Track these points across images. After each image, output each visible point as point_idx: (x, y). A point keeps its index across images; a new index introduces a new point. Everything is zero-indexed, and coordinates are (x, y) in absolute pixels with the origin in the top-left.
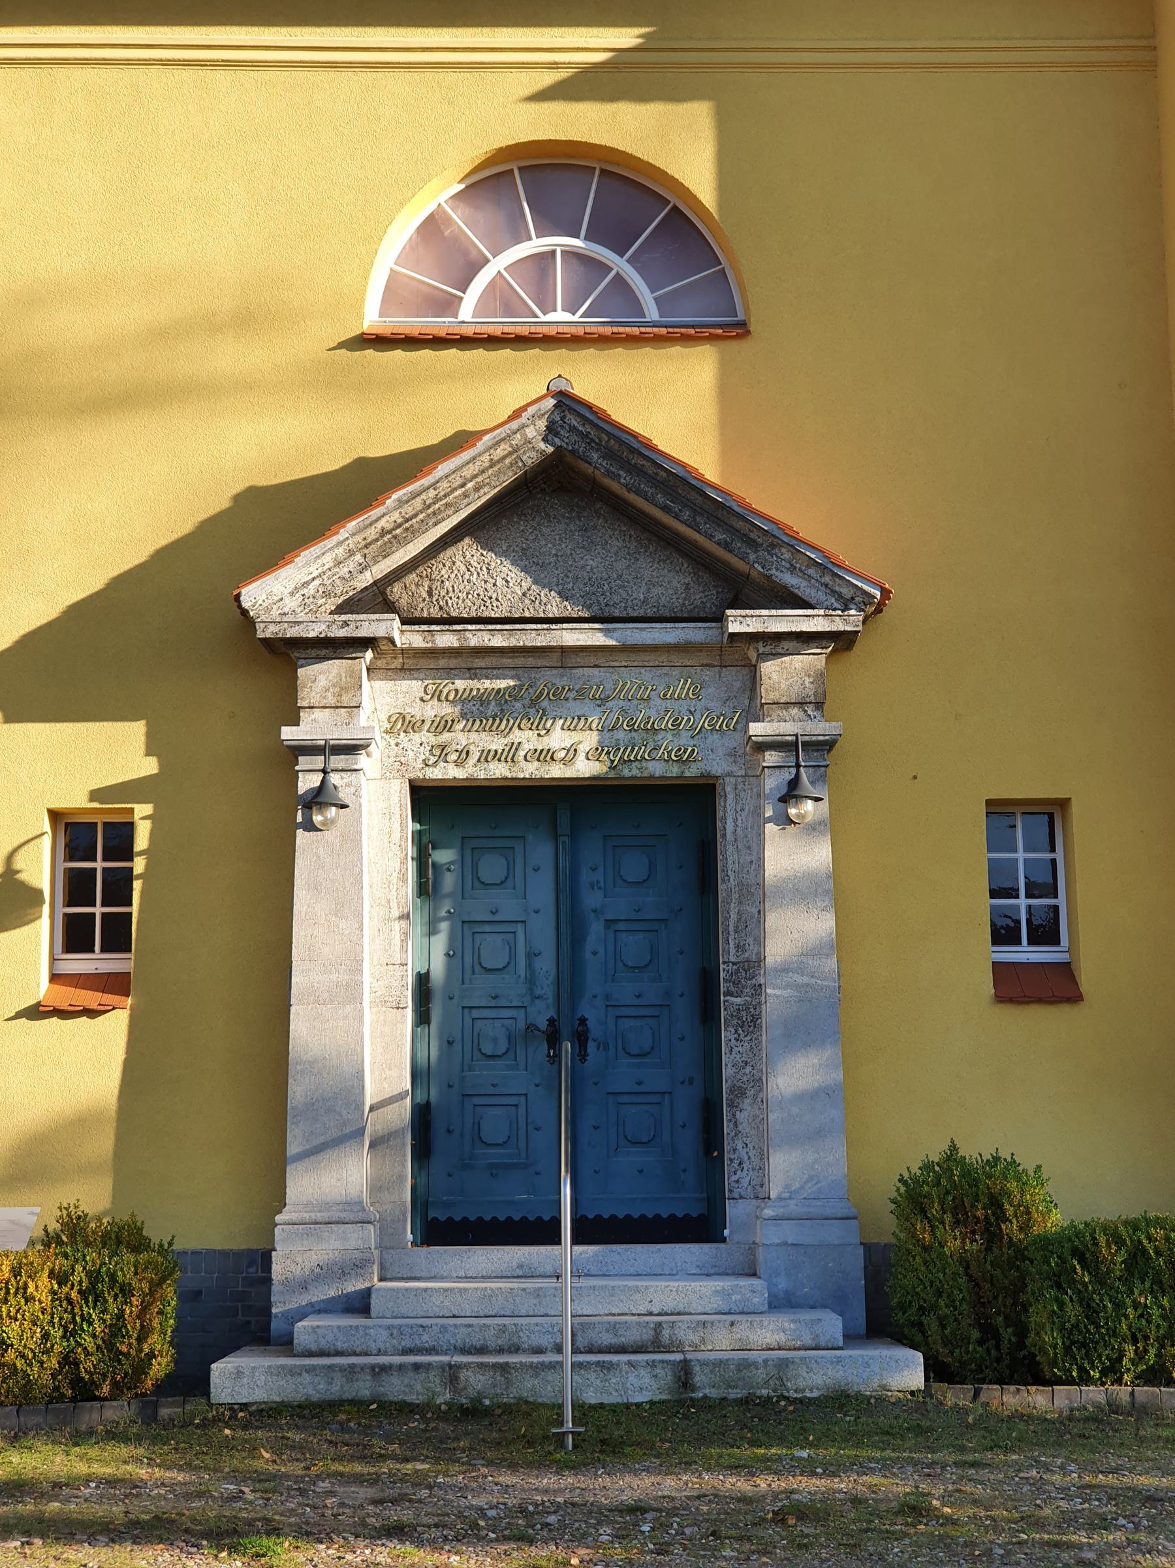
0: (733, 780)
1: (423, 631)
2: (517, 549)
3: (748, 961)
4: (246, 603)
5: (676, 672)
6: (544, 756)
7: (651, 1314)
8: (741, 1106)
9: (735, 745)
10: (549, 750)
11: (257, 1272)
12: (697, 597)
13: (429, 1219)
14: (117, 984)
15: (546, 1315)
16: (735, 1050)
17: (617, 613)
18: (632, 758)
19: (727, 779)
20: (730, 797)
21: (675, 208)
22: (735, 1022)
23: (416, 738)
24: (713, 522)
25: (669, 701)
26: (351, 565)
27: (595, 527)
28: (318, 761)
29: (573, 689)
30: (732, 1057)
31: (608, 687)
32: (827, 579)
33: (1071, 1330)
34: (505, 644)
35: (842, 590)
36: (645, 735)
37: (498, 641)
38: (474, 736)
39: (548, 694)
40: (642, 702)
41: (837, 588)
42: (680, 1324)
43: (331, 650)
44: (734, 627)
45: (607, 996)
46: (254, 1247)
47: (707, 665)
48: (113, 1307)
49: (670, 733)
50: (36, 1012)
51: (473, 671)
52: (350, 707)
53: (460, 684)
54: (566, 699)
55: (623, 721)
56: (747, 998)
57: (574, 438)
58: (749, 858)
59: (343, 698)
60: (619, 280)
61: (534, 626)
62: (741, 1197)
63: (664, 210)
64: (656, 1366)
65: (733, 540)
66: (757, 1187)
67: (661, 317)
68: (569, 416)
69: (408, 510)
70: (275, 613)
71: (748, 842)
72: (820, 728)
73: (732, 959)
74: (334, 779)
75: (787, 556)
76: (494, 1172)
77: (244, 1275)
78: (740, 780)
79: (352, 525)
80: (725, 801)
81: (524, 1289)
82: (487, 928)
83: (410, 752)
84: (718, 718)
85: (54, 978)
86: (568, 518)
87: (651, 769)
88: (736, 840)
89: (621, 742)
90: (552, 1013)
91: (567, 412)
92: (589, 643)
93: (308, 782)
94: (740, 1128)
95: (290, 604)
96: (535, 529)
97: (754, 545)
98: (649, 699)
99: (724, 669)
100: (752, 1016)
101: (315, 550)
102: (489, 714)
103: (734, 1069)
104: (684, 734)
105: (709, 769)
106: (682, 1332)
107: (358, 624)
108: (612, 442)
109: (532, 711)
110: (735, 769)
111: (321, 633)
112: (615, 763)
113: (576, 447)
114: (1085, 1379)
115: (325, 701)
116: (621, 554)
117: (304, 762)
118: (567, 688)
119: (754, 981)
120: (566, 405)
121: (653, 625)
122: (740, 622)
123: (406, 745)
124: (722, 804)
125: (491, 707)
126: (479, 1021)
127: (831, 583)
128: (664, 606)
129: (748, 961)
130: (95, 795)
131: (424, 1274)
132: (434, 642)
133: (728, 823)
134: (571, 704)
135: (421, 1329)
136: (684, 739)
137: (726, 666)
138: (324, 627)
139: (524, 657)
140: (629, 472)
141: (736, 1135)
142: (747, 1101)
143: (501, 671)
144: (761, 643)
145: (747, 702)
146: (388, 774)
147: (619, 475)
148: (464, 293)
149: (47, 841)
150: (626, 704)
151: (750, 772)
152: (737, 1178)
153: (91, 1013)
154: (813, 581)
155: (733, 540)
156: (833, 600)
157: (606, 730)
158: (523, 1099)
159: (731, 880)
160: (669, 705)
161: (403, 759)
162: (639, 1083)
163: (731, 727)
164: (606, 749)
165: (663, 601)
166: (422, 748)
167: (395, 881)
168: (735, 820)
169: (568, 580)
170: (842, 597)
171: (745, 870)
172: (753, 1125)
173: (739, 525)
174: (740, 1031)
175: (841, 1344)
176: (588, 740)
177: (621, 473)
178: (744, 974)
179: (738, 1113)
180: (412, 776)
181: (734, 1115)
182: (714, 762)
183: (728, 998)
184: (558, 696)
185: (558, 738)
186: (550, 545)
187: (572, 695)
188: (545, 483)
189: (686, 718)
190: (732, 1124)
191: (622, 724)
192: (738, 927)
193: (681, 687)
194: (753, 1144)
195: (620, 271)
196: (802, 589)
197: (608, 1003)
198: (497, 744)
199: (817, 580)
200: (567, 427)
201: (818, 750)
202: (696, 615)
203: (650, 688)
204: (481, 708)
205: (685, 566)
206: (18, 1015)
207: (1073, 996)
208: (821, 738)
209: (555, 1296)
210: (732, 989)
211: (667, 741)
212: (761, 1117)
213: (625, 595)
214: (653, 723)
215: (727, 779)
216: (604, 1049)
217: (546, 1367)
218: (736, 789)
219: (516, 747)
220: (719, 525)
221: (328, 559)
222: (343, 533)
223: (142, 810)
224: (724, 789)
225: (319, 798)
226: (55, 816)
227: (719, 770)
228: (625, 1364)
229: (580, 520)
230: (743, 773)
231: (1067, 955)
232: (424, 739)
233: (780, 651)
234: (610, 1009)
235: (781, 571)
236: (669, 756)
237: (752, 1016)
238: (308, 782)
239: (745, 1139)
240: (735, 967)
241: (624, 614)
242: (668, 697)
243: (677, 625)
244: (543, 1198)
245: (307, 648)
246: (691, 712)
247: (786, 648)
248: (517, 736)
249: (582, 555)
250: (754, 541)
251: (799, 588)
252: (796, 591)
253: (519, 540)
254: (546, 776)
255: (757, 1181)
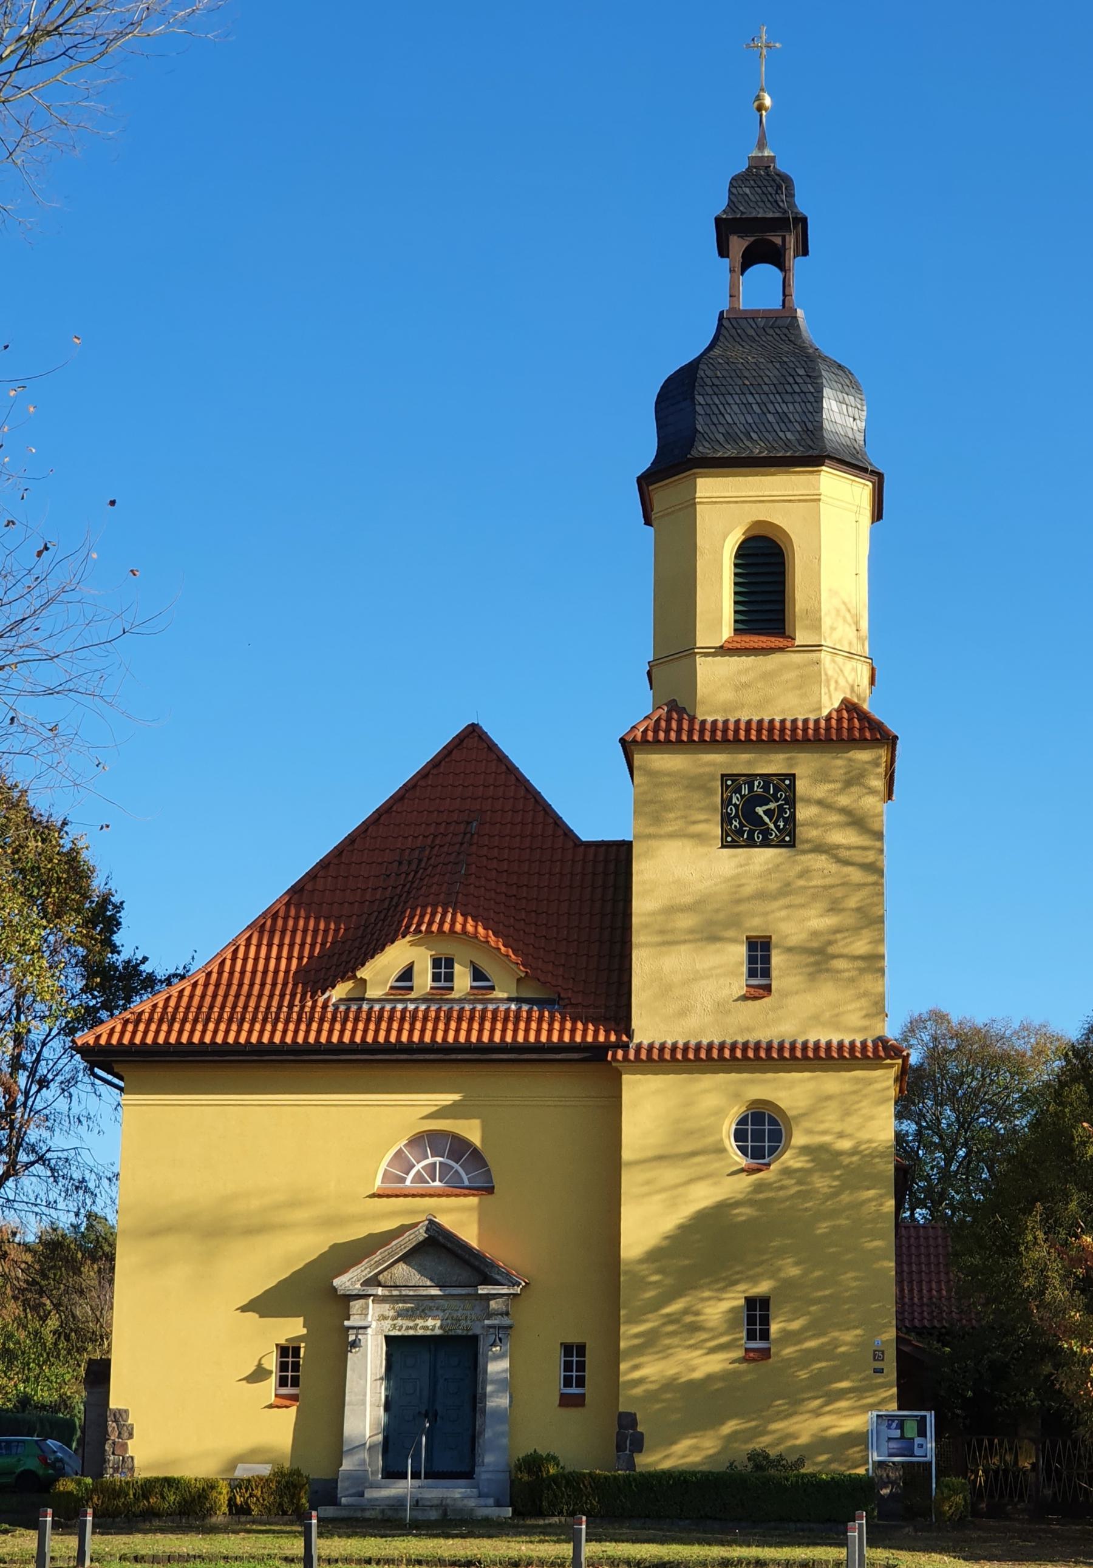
4: (335, 1284)
6: (426, 1328)
14: (294, 1398)
23: (387, 1322)
26: (366, 1272)
28: (354, 1331)
37: (411, 1293)
38: (404, 1322)
44: (480, 1292)
48: (292, 1490)
50: (271, 1406)
53: (400, 1305)
60: (456, 1171)
69: (383, 1255)
70: (343, 1287)
72: (506, 1321)
74: (360, 1337)
79: (366, 1260)
85: (276, 1395)
93: (352, 1338)
95: (348, 1284)
97: (487, 1266)
101: (355, 1268)
114: (554, 1515)
117: (351, 1332)
122: (483, 1290)
130: (287, 1340)
136: (469, 1322)
149: (275, 1353)
152: (478, 1460)
153: (287, 1407)
176: (438, 1323)
182: (477, 1331)
184: (431, 1309)
185: (430, 1322)
193: (468, 1306)
198: (411, 1324)
206: (265, 1407)
211: (463, 1322)
219: (417, 1325)
221: (359, 1271)
222: (364, 1263)
223: (303, 1345)
225: (354, 1344)
226: (277, 1345)
238: (352, 1338)
248: (418, 1321)
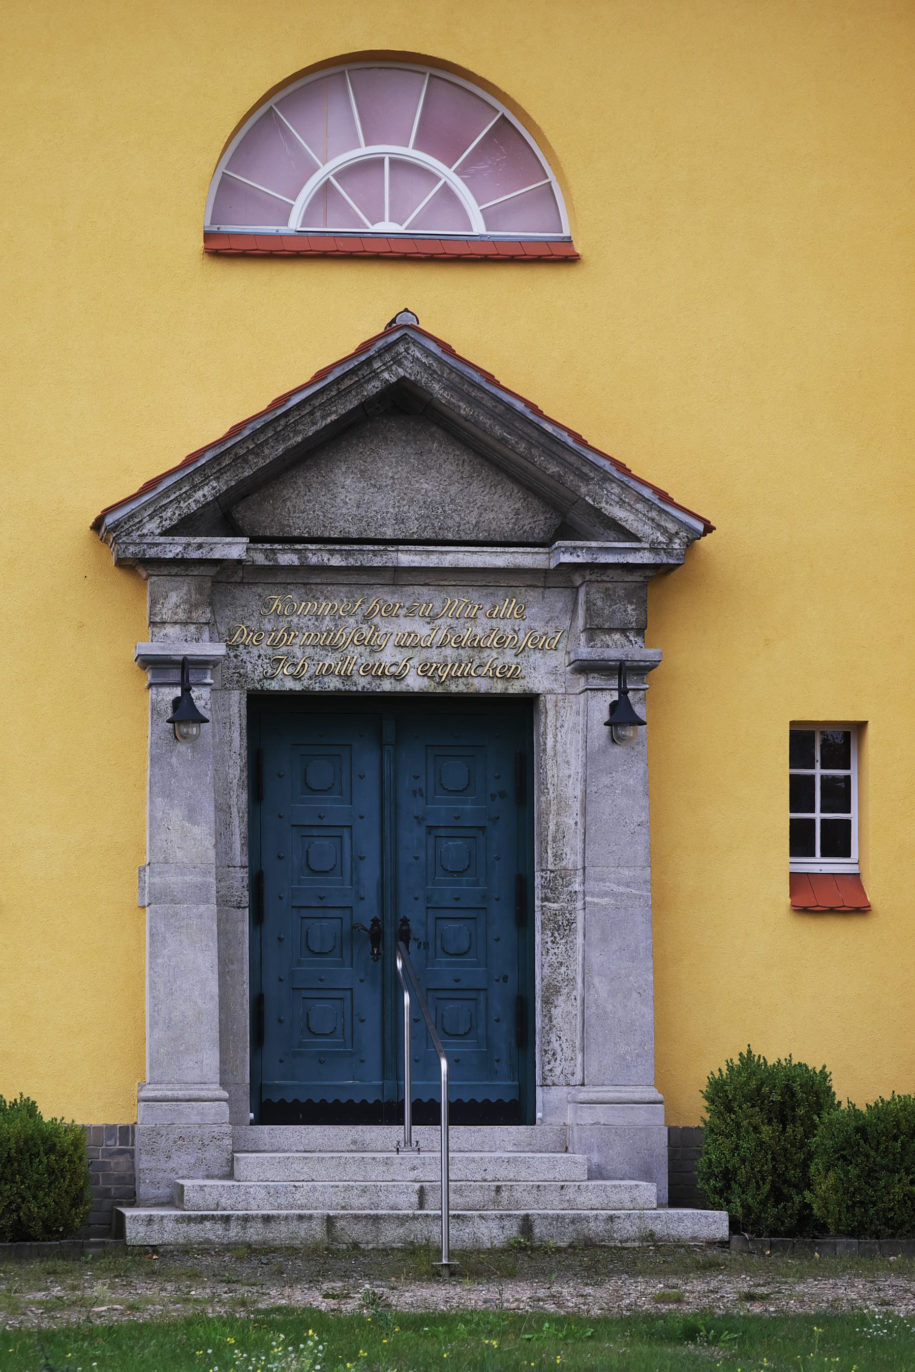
0: (553, 697)
1: (266, 549)
2: (355, 471)
3: (565, 869)
5: (501, 592)
7: (485, 1181)
8: (556, 1003)
9: (556, 663)
10: (381, 664)
11: (115, 1145)
12: (527, 522)
13: (263, 1101)
15: (393, 1180)
16: (551, 951)
17: (450, 536)
18: (459, 674)
19: (548, 697)
20: (551, 713)
21: (503, 117)
22: (551, 926)
24: (548, 454)
25: (493, 620)
27: (430, 451)
29: (404, 606)
30: (548, 958)
31: (437, 604)
32: (653, 514)
33: (854, 1193)
34: (343, 564)
35: (667, 525)
36: (470, 652)
39: (380, 610)
40: (468, 620)
41: (663, 523)
42: (518, 1187)
43: (182, 568)
45: (428, 898)
46: (111, 1122)
47: (530, 586)
49: (495, 651)
51: (308, 587)
52: (200, 623)
54: (397, 616)
55: (451, 639)
56: (563, 904)
57: (417, 368)
58: (567, 772)
59: (194, 614)
61: (371, 547)
62: (554, 1085)
63: (494, 117)
64: (503, 1219)
65: (566, 473)
66: (569, 1076)
67: (487, 230)
68: (412, 348)
71: (566, 756)
73: (550, 867)
75: (617, 490)
76: (323, 1059)
77: (104, 1147)
78: (560, 697)
80: (546, 717)
81: (374, 1158)
82: (315, 832)
83: (248, 664)
84: (542, 638)
86: (404, 441)
87: (477, 685)
88: (555, 754)
89: (449, 659)
90: (376, 914)
91: (411, 345)
92: (423, 565)
94: (555, 1022)
96: (373, 451)
98: (475, 618)
99: (547, 590)
100: (568, 920)
102: (324, 629)
103: (550, 968)
104: (508, 651)
105: (531, 686)
106: (519, 1194)
107: (212, 546)
108: (453, 375)
109: (365, 626)
110: (555, 686)
111: (177, 554)
112: (443, 679)
113: (419, 377)
115: (177, 617)
116: (455, 478)
118: (398, 605)
119: (570, 888)
120: (412, 338)
121: (485, 549)
123: (245, 658)
124: (543, 720)
125: (326, 622)
126: (307, 921)
127: (657, 518)
128: (494, 530)
129: (565, 869)
131: (266, 1148)
132: (276, 560)
133: (548, 737)
134: (402, 620)
135: (294, 1189)
137: (549, 587)
138: (180, 549)
139: (358, 574)
140: (469, 403)
141: (551, 1029)
142: (561, 998)
143: (335, 587)
144: (588, 572)
145: (568, 623)
146: (228, 685)
147: (459, 406)
148: (294, 201)
150: (453, 622)
151: (570, 691)
154: (640, 515)
155: (566, 473)
156: (659, 534)
157: (435, 647)
158: (348, 993)
159: (551, 792)
160: (494, 623)
161: (242, 671)
162: (457, 981)
163: (553, 647)
164: (435, 665)
165: (494, 526)
166: (260, 661)
167: (235, 788)
168: (555, 736)
169: (405, 503)
170: (667, 532)
171: (564, 784)
172: (566, 1020)
173: (572, 459)
174: (556, 935)
175: (655, 1206)
177: (461, 404)
178: (560, 881)
179: (553, 1009)
180: (250, 687)
181: (549, 1011)
183: (546, 903)
186: (387, 468)
187: (403, 612)
188: (379, 403)
189: (510, 637)
190: (547, 1019)
191: (450, 641)
192: (555, 837)
194: (565, 1037)
195: (448, 181)
196: (629, 522)
197: (429, 905)
199: (644, 515)
200: (411, 358)
201: (638, 675)
202: (525, 540)
203: (477, 607)
204: (316, 623)
205: (516, 491)
207: (862, 910)
208: (642, 663)
209: (401, 1164)
210: (550, 895)
212: (574, 1012)
213: (458, 519)
214: (479, 641)
215: (548, 697)
216: (424, 949)
217: (411, 1218)
218: (556, 706)
220: (553, 458)
224: (545, 706)
227: (541, 688)
228: (478, 1217)
229: (416, 443)
230: (563, 690)
231: (856, 867)
232: (262, 652)
233: (605, 578)
234: (429, 910)
235: (611, 505)
236: (494, 673)
237: (568, 920)
239: (558, 1032)
240: (552, 875)
241: (457, 538)
242: (494, 616)
243: (507, 549)
244: (368, 1083)
245: (160, 566)
246: (515, 631)
247: (611, 576)
249: (417, 479)
250: (586, 474)
251: (627, 521)
252: (624, 524)
253: (357, 462)
254: (378, 690)
255: (570, 1070)
